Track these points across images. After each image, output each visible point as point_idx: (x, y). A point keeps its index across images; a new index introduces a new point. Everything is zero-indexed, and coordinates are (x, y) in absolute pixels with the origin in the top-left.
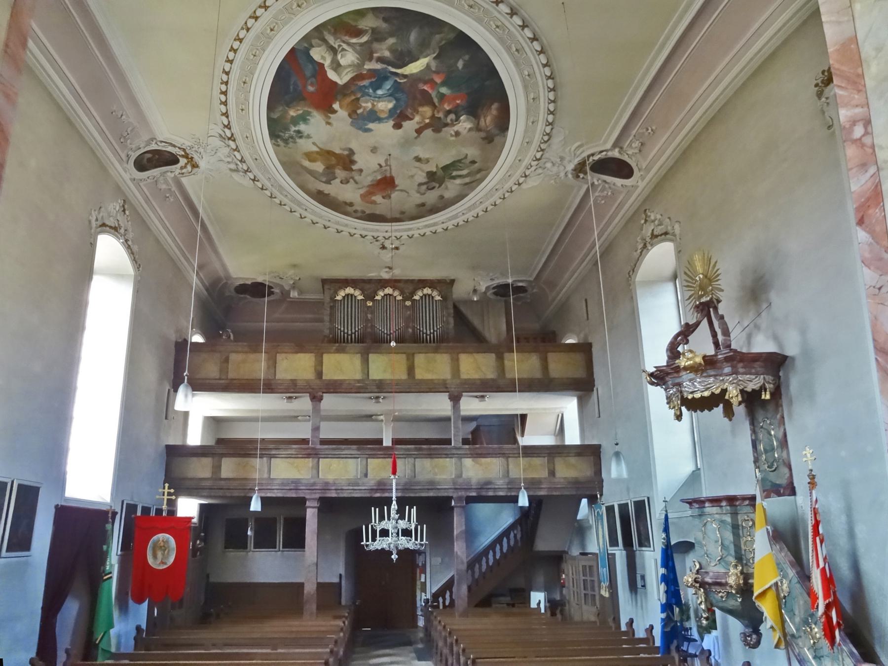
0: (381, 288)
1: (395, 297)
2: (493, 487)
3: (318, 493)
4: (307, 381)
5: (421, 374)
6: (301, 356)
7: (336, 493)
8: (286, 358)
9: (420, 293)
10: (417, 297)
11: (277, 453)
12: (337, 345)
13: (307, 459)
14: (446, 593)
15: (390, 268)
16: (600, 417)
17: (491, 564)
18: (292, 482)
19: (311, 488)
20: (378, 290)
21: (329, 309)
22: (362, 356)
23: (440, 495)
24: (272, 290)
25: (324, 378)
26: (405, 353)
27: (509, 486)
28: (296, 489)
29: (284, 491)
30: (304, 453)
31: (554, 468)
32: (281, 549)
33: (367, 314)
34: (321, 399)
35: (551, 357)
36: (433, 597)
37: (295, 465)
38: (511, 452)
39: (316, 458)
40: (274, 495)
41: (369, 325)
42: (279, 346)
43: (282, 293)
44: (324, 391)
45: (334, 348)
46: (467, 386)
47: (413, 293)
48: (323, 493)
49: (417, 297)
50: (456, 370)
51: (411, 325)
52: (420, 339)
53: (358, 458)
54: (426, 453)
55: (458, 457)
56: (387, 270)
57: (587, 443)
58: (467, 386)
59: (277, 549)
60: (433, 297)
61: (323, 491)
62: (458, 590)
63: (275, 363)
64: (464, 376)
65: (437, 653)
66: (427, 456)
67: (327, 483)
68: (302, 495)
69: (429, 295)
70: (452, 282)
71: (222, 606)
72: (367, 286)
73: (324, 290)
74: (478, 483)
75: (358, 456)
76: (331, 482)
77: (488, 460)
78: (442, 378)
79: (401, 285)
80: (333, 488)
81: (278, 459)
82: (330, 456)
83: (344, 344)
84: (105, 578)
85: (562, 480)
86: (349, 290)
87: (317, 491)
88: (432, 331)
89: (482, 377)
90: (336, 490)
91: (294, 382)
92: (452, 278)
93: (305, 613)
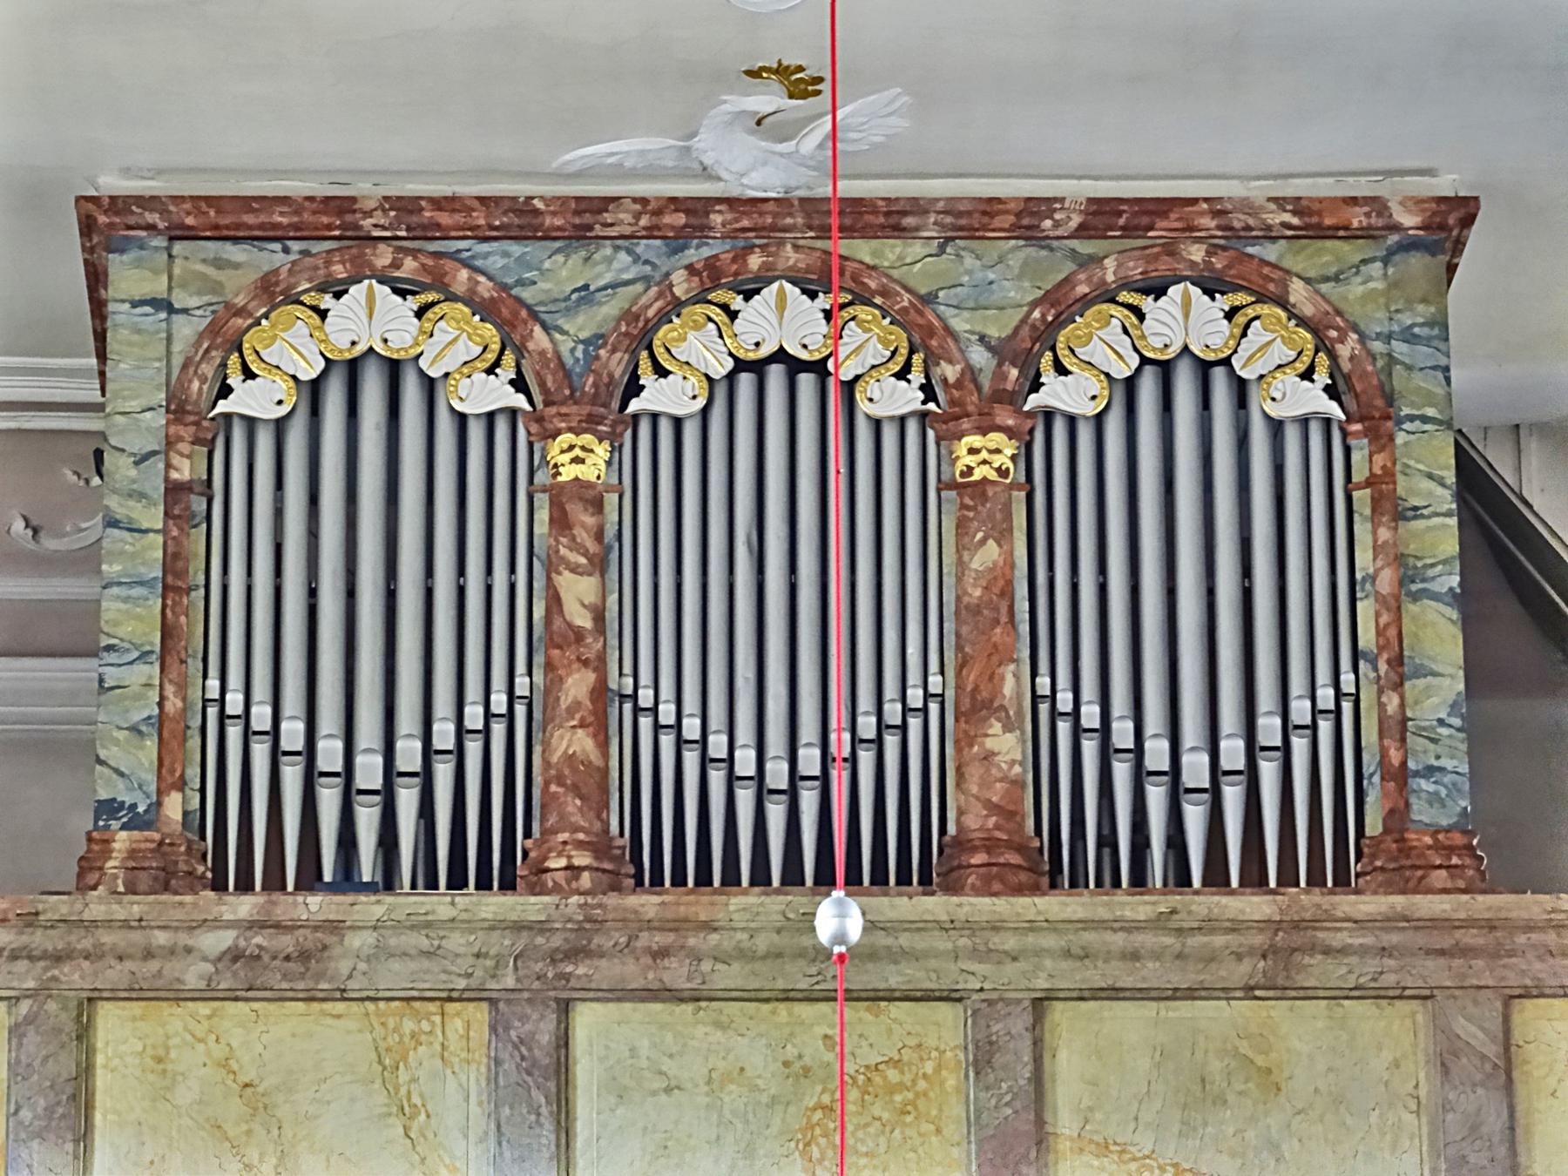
12: (244, 906)
15: (800, 85)
21: (153, 517)
26: (951, 997)
41: (577, 685)
51: (1012, 684)
52: (1107, 840)
56: (769, 99)
60: (1241, 388)
69: (394, 368)
73: (98, 309)
83: (315, 902)
84: (931, 434)
88: (1233, 752)
92: (1446, 185)
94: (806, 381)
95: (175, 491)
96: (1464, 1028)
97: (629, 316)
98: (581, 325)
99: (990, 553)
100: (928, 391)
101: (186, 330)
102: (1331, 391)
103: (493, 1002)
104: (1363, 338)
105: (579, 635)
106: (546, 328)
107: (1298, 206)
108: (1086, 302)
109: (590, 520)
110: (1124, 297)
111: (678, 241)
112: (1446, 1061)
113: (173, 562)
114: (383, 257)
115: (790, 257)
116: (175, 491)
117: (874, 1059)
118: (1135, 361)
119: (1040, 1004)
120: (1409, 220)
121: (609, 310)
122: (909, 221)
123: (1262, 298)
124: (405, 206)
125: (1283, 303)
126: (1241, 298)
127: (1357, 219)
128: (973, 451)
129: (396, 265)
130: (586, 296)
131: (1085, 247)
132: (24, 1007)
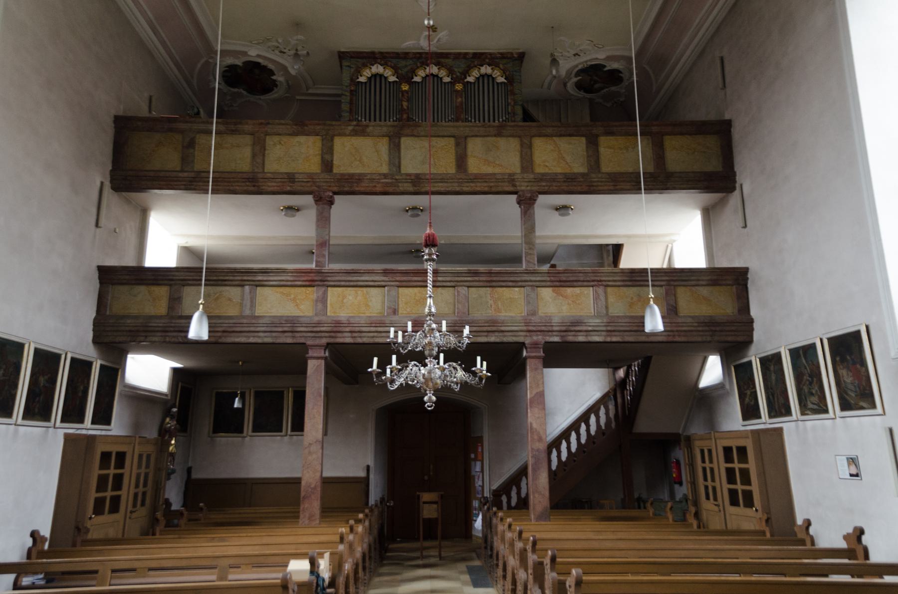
0: (421, 66)
1: (441, 78)
2: (585, 328)
3: (326, 337)
4: (311, 176)
5: (475, 166)
6: (302, 139)
7: (352, 337)
8: (280, 143)
9: (475, 73)
10: (470, 79)
11: (265, 278)
13: (310, 289)
14: (511, 489)
16: (745, 226)
17: (583, 441)
18: (287, 321)
19: (315, 329)
20: (418, 67)
22: (390, 140)
23: (505, 340)
24: (274, 78)
25: (335, 171)
27: (609, 328)
28: (292, 332)
29: (274, 334)
30: (305, 279)
31: (676, 302)
32: (289, 433)
33: (402, 101)
34: (331, 203)
35: (670, 142)
36: (493, 495)
37: (292, 296)
38: (611, 279)
39: (323, 285)
40: (259, 341)
42: (268, 123)
43: (288, 84)
44: (336, 189)
45: (350, 128)
46: (544, 184)
47: (466, 73)
48: (332, 337)
49: (470, 79)
50: (527, 162)
53: (384, 286)
54: (484, 279)
55: (531, 286)
57: (725, 264)
58: (544, 184)
59: (283, 433)
60: (493, 79)
61: (332, 334)
62: (535, 478)
63: (263, 148)
64: (539, 170)
65: (504, 577)
66: (486, 284)
67: (338, 323)
68: (302, 341)
70: (522, 56)
71: (201, 504)
72: (402, 63)
74: (562, 324)
75: (383, 283)
76: (344, 320)
77: (577, 290)
78: (508, 171)
79: (449, 61)
80: (347, 329)
81: (266, 289)
82: (343, 283)
85: (690, 320)
86: (377, 69)
87: (323, 334)
89: (568, 171)
90: (351, 332)
91: (291, 178)
93: (301, 516)
94: (436, 78)
95: (351, 91)
96: (526, 141)
97: (412, 68)
98: (406, 70)
99: (460, 100)
100: (452, 79)
101: (352, 70)
102: (505, 79)
103: (389, 137)
104: (510, 72)
105: (405, 109)
106: (401, 70)
107: (501, 54)
108: (472, 68)
109: (407, 95)
110: (478, 66)
111: (419, 58)
112: (522, 146)
113: (351, 100)
114: (379, 61)
115: (433, 61)
116: (351, 91)
117: (443, 145)
118: (479, 75)
119: (466, 137)
120: (516, 56)
121: (409, 68)
122: (449, 56)
123: (496, 67)
124: (381, 53)
125: (499, 67)
126: (493, 67)
127: (509, 56)
128: (458, 86)
129: (381, 62)
130: (406, 66)
131: (472, 60)
132: (324, 137)
